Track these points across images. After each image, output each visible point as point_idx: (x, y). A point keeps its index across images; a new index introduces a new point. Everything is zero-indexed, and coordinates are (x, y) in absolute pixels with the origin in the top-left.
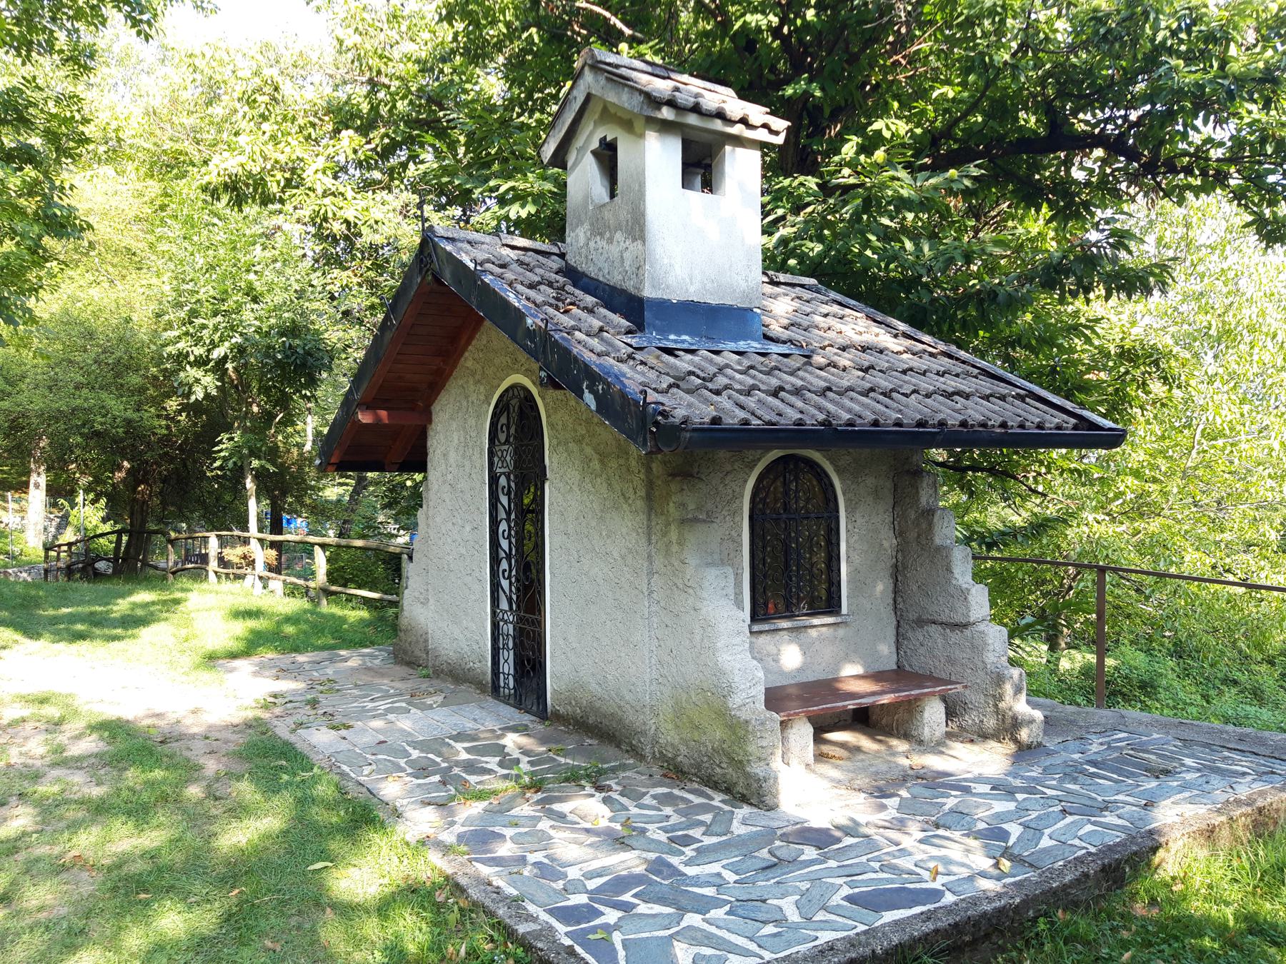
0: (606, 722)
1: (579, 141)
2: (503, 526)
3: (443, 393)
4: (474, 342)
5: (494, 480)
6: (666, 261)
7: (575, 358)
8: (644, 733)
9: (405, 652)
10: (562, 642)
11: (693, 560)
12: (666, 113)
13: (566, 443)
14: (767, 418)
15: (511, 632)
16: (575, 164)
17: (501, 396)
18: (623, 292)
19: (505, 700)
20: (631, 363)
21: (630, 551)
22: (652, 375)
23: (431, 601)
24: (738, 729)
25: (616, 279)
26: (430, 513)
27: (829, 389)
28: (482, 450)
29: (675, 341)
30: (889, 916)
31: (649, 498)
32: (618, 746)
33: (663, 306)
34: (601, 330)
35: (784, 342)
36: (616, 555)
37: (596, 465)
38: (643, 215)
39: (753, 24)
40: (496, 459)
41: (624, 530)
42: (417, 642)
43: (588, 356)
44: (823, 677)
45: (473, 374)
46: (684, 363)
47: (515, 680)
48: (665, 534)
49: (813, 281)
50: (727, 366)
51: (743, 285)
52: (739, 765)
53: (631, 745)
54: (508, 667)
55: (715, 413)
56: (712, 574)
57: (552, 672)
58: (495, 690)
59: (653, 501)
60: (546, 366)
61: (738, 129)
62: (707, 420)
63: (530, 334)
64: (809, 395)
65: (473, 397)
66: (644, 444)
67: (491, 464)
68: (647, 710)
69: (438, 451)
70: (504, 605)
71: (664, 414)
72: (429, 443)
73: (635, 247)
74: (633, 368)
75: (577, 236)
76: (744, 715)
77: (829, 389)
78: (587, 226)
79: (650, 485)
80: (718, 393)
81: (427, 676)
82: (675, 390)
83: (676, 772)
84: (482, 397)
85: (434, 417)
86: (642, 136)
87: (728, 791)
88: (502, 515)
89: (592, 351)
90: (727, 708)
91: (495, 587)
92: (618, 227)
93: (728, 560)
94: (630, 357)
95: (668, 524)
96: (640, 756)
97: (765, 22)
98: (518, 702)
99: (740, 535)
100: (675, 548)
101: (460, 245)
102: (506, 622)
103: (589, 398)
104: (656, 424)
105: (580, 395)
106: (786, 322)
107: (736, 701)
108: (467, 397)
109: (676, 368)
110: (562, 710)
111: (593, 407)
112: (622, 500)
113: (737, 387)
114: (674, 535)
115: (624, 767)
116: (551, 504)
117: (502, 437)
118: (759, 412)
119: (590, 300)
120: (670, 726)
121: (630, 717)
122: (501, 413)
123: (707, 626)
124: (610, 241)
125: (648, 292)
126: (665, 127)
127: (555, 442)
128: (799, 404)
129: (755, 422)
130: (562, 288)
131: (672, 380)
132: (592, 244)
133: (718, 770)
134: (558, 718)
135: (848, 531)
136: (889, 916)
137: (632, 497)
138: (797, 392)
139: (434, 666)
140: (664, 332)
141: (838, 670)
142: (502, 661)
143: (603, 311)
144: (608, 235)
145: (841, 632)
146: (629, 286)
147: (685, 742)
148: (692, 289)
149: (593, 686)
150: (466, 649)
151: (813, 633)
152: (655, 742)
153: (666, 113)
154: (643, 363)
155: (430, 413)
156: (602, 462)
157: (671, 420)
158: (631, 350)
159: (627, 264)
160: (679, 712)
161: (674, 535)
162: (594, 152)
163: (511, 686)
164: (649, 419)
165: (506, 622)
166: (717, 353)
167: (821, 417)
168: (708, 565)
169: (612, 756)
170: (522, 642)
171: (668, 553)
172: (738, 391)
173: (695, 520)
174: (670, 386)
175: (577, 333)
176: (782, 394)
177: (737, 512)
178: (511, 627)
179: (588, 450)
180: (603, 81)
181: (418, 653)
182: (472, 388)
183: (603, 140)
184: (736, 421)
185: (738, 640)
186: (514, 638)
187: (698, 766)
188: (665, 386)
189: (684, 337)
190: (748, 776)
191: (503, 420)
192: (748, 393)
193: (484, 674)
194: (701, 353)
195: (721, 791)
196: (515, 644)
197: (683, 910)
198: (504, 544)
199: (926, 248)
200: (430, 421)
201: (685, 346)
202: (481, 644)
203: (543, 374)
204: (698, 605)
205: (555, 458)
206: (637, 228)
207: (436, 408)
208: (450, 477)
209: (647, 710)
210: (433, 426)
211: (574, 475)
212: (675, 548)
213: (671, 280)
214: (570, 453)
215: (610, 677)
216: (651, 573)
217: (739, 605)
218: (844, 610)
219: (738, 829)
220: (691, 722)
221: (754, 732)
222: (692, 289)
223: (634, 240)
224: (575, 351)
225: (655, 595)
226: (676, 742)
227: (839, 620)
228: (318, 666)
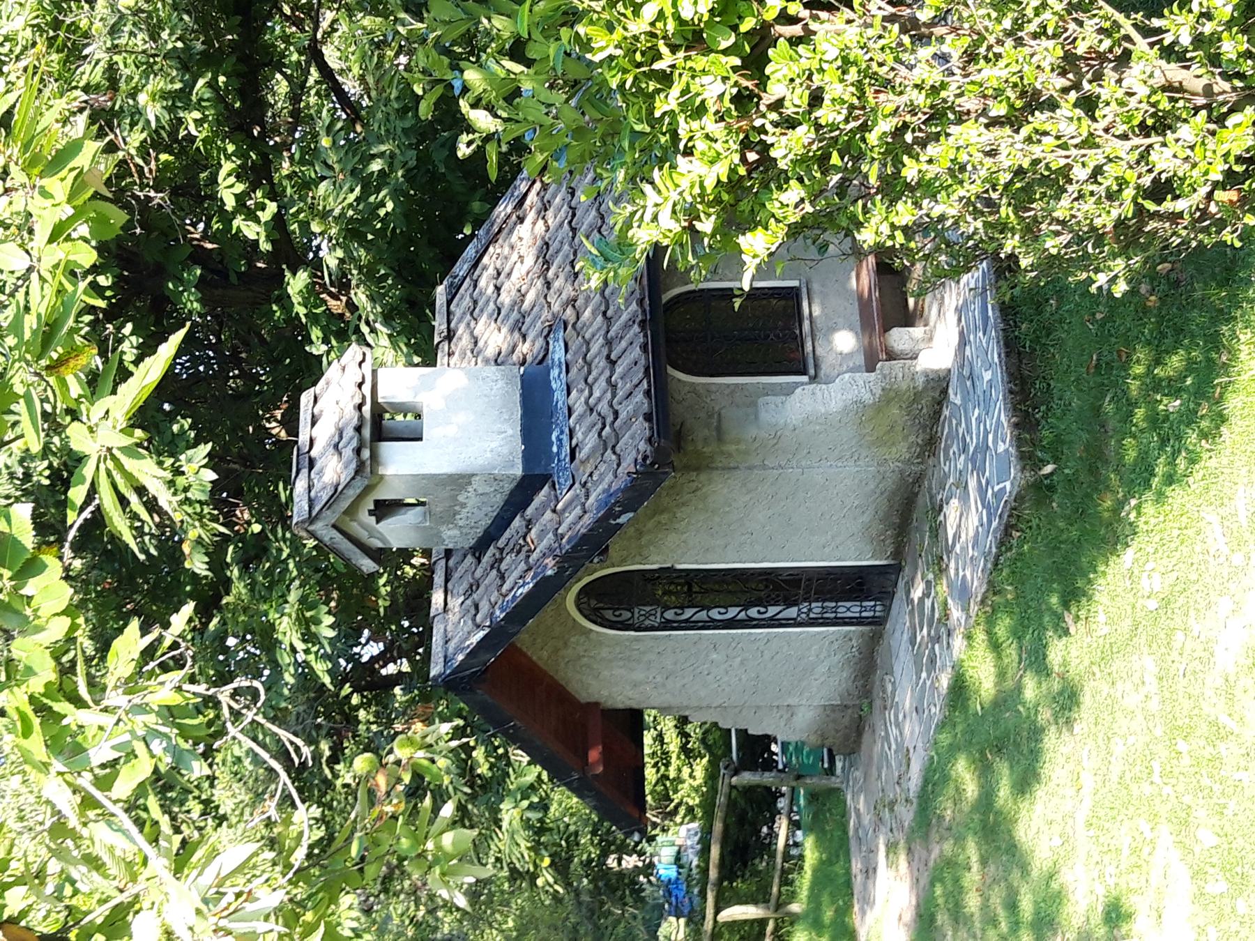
0: (896, 506)
1: (363, 535)
2: (715, 614)
3: (569, 689)
4: (525, 650)
5: (667, 625)
6: (489, 455)
7: (590, 530)
8: (901, 472)
9: (846, 737)
10: (827, 550)
11: (753, 432)
12: (366, 454)
13: (641, 547)
14: (641, 375)
15: (820, 604)
16: (383, 539)
17: (586, 617)
18: (512, 493)
19: (887, 609)
20: (589, 485)
21: (744, 485)
22: (602, 468)
23: (790, 701)
24: (889, 396)
25: (499, 500)
26: (694, 703)
27: (604, 313)
28: (637, 639)
29: (560, 446)
30: (990, 313)
31: (698, 469)
32: (916, 494)
33: (528, 457)
34: (554, 511)
35: (548, 343)
36: (747, 498)
37: (664, 518)
38: (450, 476)
39: (135, 351)
40: (647, 622)
41: (726, 491)
42: (834, 721)
43: (588, 520)
44: (635, 706)
45: (556, 650)
46: (589, 442)
47: (867, 599)
48: (730, 455)
49: (441, 291)
50: (587, 402)
51: (500, 384)
52: (918, 396)
53: (914, 483)
54: (850, 609)
55: (641, 419)
56: (765, 416)
57: (856, 559)
58: (878, 622)
59: (702, 465)
60: (590, 558)
61: (367, 389)
62: (646, 425)
63: (561, 570)
64: (611, 334)
65: (580, 650)
66: (666, 473)
67: (652, 629)
68: (882, 469)
69: (630, 694)
70: (792, 612)
71: (645, 458)
72: (621, 706)
73: (476, 483)
74: (596, 484)
75: (449, 537)
76: (879, 392)
77: (604, 313)
78: (443, 528)
79: (687, 468)
80: (616, 414)
81: (870, 705)
82: (618, 449)
83: (930, 445)
84: (583, 639)
85: (592, 700)
86: (382, 477)
87: (940, 403)
88: (703, 615)
89: (580, 518)
90: (874, 404)
91: (774, 622)
92: (454, 498)
93: (751, 401)
94: (584, 485)
95: (722, 453)
96: (919, 479)
97: (133, 339)
98: (886, 596)
99: (728, 386)
100: (742, 447)
101: (451, 650)
102: (810, 610)
103: (623, 519)
104: (652, 464)
105: (620, 526)
106: (516, 335)
107: (867, 398)
108: (579, 657)
109: (594, 450)
110: (890, 550)
111: (631, 515)
112: (699, 493)
113: (609, 395)
114: (732, 448)
115: (930, 488)
116: (697, 563)
117: (627, 615)
118: (635, 381)
119: (517, 522)
120: (894, 450)
121: (890, 483)
122: (603, 618)
123: (808, 420)
124: (463, 505)
125: (518, 471)
126: (374, 457)
127: (638, 558)
128: (624, 344)
129: (645, 384)
130: (501, 550)
131: (609, 451)
132: (461, 523)
133: (925, 411)
134: (898, 553)
135: (721, 280)
136: (990, 313)
137: (696, 484)
138: (609, 343)
139: (859, 697)
140: (550, 457)
141: (852, 291)
142: (849, 614)
143: (530, 511)
144: (457, 508)
145: (815, 287)
146: (508, 487)
147: (906, 438)
148: (510, 432)
149: (866, 518)
150: (839, 656)
151: (817, 311)
152: (908, 462)
153: (366, 454)
154: (591, 475)
155: (588, 704)
156: (662, 512)
157: (648, 453)
158: (577, 485)
159: (488, 489)
160: (880, 442)
161: (732, 448)
162: (378, 522)
163: (872, 603)
164: (650, 470)
165: (810, 610)
166: (570, 412)
167: (636, 328)
168: (757, 418)
169: (923, 500)
170: (830, 592)
171: (747, 453)
172: (614, 395)
173: (719, 429)
174: (614, 453)
175: (560, 531)
176: (613, 357)
177: (708, 389)
178: (813, 605)
179: (650, 524)
180: (328, 512)
181: (846, 721)
182: (570, 651)
183: (371, 513)
184: (645, 401)
185: (819, 394)
186: (824, 601)
187: (924, 427)
188: (614, 457)
189: (554, 438)
190: (925, 389)
191: (609, 614)
192: (614, 387)
193: (863, 634)
194: (572, 425)
195: (941, 408)
196: (831, 600)
197: (988, 447)
198: (732, 612)
199: (383, 148)
200: (597, 704)
201: (565, 438)
202: (832, 638)
203: (596, 560)
204: (791, 427)
205: (653, 558)
206: (459, 481)
207: (583, 697)
208: (659, 679)
209: (882, 469)
210: (602, 701)
211: (672, 539)
212: (742, 447)
213: (505, 451)
214: (650, 543)
215: (857, 503)
216: (764, 467)
217: (789, 390)
218: (795, 283)
219: (958, 401)
220: (889, 432)
221: (891, 384)
222: (510, 432)
223: (470, 483)
224: (583, 531)
225: (783, 463)
226: (906, 445)
227: (804, 290)
228: (864, 841)
